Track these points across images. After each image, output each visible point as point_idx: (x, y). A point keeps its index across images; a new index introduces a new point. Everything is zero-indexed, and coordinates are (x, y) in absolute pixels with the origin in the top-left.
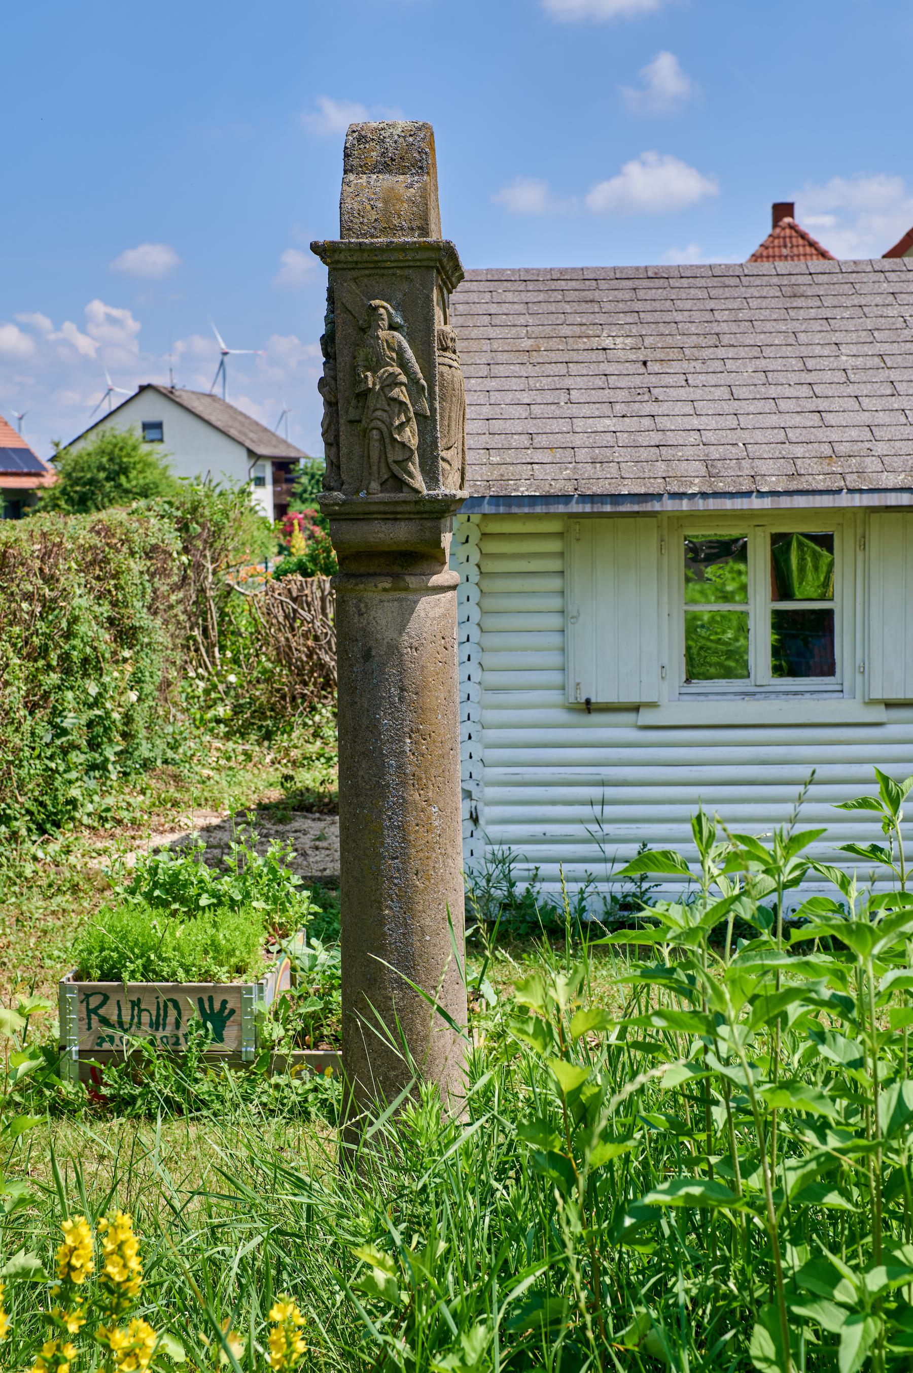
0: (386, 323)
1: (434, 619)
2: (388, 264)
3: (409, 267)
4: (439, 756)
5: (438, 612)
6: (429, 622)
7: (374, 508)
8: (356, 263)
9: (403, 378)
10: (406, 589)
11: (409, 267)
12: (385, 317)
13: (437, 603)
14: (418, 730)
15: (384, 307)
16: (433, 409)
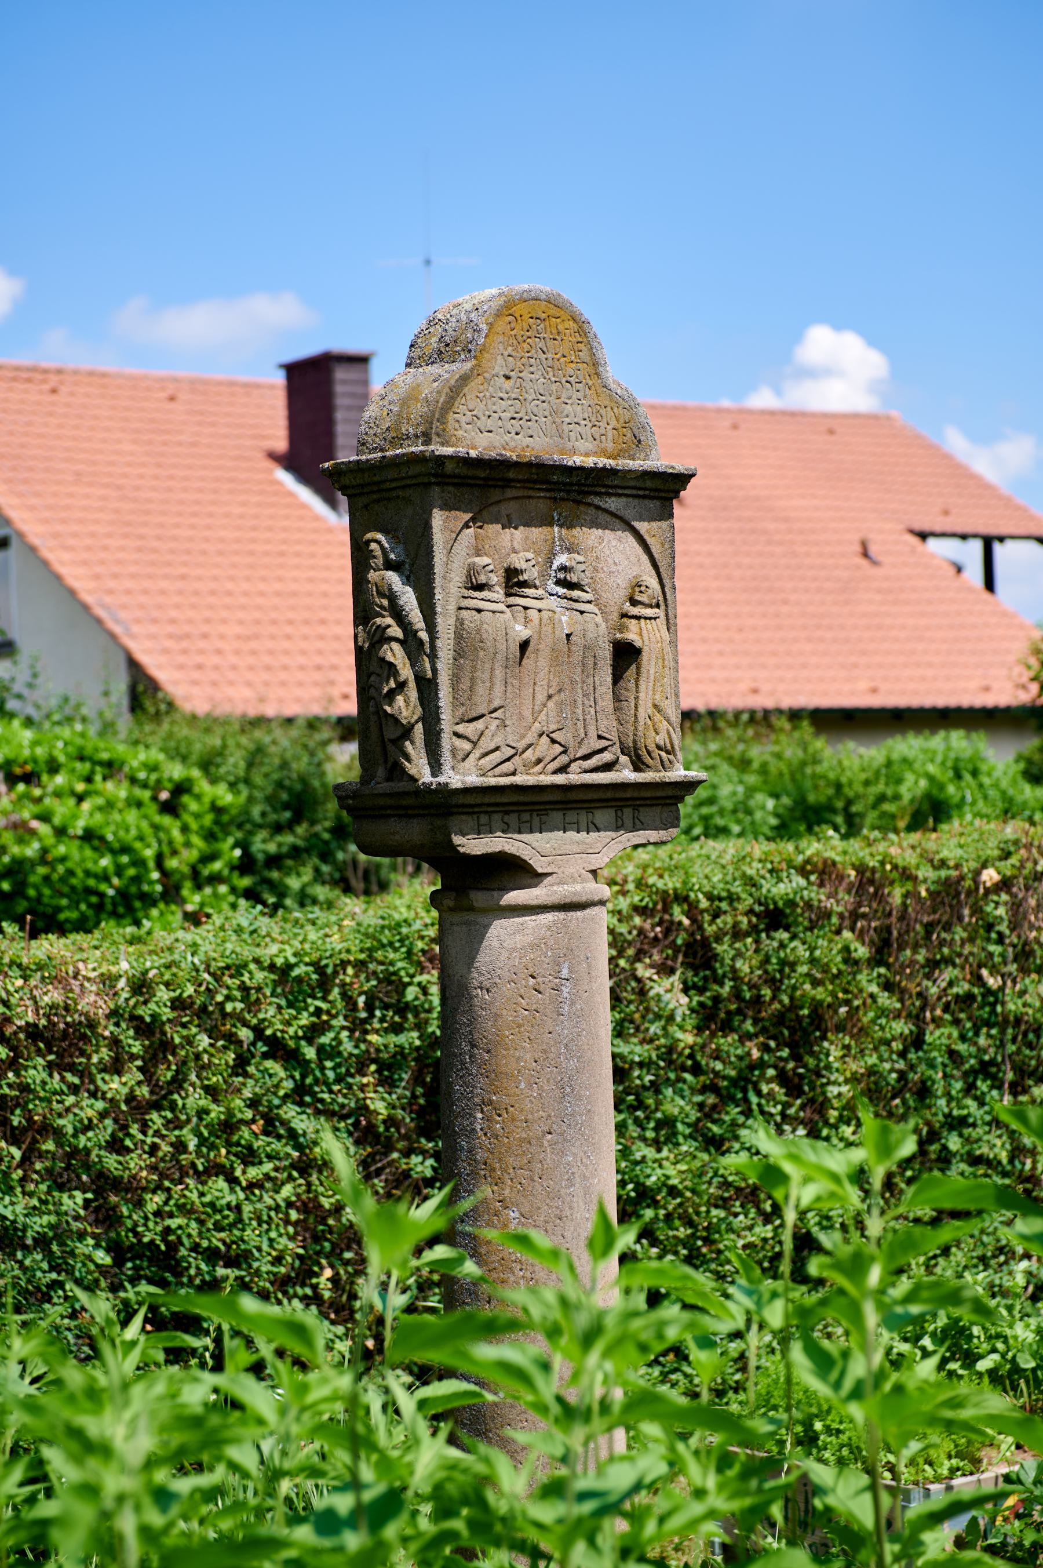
0: (380, 561)
1: (514, 950)
2: (388, 485)
3: (409, 486)
4: (522, 1140)
5: (520, 940)
6: (505, 954)
7: (381, 802)
8: (362, 486)
9: (395, 631)
10: (471, 909)
11: (409, 486)
12: (378, 553)
13: (521, 930)
14: (491, 1103)
15: (378, 542)
16: (434, 670)
